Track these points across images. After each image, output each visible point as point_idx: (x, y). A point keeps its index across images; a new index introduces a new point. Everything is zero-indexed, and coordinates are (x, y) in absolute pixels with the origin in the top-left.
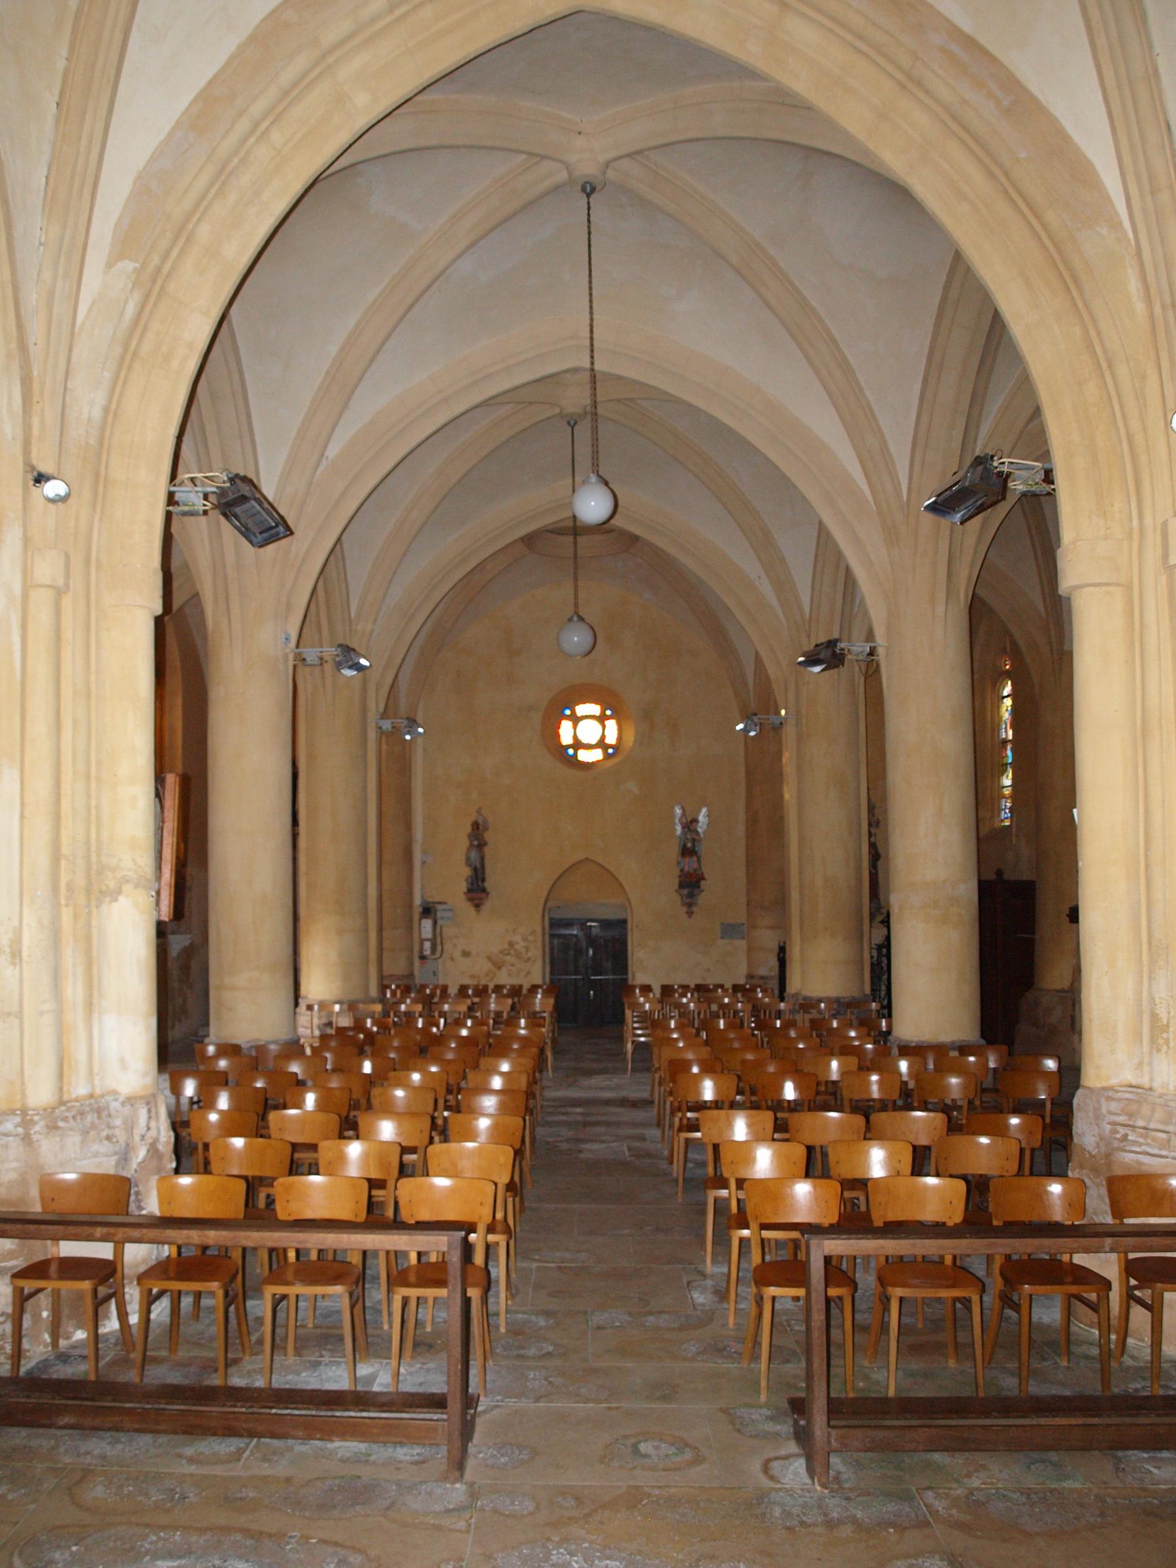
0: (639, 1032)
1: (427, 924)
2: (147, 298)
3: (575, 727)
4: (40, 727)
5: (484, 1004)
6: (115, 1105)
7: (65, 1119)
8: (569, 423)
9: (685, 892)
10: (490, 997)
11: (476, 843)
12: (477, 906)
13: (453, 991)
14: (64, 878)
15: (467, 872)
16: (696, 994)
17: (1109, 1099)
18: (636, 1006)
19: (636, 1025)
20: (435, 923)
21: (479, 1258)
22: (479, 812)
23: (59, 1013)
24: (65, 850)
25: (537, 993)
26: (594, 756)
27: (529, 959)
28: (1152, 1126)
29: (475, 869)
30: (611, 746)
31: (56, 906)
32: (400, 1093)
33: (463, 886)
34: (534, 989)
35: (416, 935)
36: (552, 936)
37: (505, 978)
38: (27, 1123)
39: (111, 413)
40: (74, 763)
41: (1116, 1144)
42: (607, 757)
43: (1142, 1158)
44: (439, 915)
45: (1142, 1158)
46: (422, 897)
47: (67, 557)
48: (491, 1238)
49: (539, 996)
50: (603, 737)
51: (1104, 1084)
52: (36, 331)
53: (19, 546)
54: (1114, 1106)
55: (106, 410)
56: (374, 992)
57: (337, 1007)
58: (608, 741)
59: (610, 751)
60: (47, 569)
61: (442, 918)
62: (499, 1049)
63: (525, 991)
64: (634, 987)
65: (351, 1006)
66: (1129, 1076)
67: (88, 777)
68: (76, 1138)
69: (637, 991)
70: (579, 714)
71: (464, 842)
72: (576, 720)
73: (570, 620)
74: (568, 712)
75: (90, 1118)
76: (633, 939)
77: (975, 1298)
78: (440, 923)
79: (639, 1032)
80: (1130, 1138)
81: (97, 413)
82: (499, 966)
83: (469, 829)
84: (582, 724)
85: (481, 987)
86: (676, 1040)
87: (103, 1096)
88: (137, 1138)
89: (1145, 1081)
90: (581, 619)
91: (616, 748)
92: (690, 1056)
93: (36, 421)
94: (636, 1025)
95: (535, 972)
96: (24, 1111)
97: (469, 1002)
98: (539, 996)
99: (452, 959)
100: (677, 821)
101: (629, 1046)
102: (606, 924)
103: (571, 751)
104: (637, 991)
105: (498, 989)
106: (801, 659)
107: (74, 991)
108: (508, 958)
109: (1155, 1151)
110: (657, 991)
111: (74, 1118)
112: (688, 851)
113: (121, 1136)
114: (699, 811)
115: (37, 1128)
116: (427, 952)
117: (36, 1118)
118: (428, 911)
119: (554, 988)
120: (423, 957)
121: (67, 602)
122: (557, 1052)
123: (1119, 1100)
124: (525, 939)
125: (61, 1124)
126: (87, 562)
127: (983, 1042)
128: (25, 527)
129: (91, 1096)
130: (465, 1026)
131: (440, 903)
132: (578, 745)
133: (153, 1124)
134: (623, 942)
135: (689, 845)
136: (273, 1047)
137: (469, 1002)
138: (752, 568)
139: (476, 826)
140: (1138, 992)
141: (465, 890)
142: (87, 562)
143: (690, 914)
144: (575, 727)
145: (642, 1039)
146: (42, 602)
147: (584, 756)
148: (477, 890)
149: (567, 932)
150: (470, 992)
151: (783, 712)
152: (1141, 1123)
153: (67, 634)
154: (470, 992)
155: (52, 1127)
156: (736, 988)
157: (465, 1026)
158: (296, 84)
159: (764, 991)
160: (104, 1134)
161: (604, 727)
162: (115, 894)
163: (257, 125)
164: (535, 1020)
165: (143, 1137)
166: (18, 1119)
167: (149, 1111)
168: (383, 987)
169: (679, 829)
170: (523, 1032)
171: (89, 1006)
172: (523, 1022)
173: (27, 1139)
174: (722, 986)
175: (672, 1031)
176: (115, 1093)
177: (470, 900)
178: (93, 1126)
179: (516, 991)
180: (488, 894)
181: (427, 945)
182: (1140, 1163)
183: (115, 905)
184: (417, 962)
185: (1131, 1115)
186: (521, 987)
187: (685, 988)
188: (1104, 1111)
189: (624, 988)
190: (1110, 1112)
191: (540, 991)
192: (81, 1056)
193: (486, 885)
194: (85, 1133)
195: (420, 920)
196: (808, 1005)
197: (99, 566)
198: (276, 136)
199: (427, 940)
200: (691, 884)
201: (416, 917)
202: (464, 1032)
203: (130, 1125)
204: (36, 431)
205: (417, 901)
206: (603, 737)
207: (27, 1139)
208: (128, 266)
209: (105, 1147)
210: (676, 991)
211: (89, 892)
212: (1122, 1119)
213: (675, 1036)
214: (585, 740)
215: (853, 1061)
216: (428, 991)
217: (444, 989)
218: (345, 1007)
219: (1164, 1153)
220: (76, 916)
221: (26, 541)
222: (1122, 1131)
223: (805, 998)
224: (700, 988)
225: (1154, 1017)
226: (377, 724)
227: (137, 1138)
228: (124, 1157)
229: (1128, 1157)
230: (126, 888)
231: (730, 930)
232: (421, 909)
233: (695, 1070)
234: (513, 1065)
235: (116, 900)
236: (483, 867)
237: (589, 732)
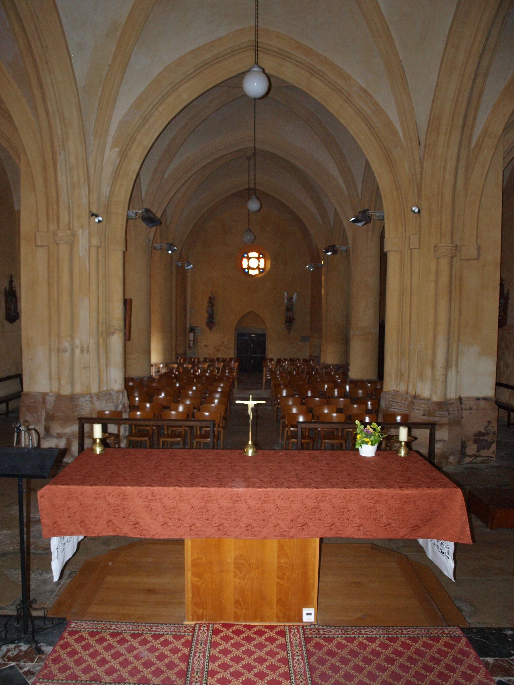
0: (268, 375)
1: (192, 335)
2: (122, 157)
3: (248, 261)
4: (93, 287)
5: (213, 365)
6: (113, 393)
7: (102, 396)
8: (248, 159)
9: (287, 324)
10: (215, 362)
11: (210, 305)
12: (210, 328)
13: (202, 360)
14: (100, 329)
15: (207, 315)
16: (289, 362)
17: (389, 394)
18: (267, 366)
19: (267, 373)
20: (194, 334)
21: (216, 433)
22: (212, 293)
23: (99, 367)
24: (100, 321)
25: (232, 361)
26: (256, 272)
27: (229, 348)
28: (398, 401)
29: (210, 315)
30: (262, 269)
31: (98, 338)
32: (190, 392)
33: (205, 321)
34: (231, 359)
35: (187, 339)
36: (238, 340)
37: (220, 355)
38: (91, 397)
39: (112, 193)
40: (103, 297)
41: (389, 406)
42: (260, 272)
43: (395, 410)
44: (196, 331)
45: (395, 410)
46: (190, 324)
47: (101, 238)
48: (219, 429)
49: (233, 362)
50: (259, 265)
51: (388, 390)
52: (92, 171)
53: (88, 235)
54: (390, 396)
55: (110, 192)
56: (174, 360)
57: (161, 366)
58: (260, 267)
59: (261, 270)
60: (95, 241)
61: (197, 333)
62: (220, 379)
63: (227, 360)
64: (267, 360)
65: (166, 365)
66: (394, 388)
67: (106, 300)
68: (105, 402)
69: (268, 361)
70: (250, 256)
71: (206, 304)
72: (249, 258)
73: (247, 231)
74: (246, 255)
75: (108, 396)
76: (268, 341)
77: (344, 443)
78: (196, 334)
79: (268, 375)
80: (393, 404)
81: (108, 194)
82: (218, 351)
83: (208, 300)
84: (251, 260)
85: (212, 358)
86: (278, 378)
87: (110, 390)
88: (119, 402)
89: (398, 389)
90: (250, 231)
91: (263, 269)
92: (281, 382)
93: (91, 197)
94: (267, 373)
95: (231, 353)
96: (90, 394)
97: (208, 364)
98: (233, 362)
99: (201, 348)
100: (285, 298)
101: (264, 380)
102: (258, 335)
103: (246, 270)
104: (268, 361)
105: (218, 359)
106: (324, 250)
107: (103, 361)
108: (222, 348)
109: (398, 408)
110: (275, 360)
111: (104, 396)
112: (289, 309)
113: (115, 401)
114: (294, 294)
115: (94, 399)
116: (192, 345)
117: (94, 396)
118: (192, 330)
119: (239, 359)
120: (190, 347)
121: (100, 250)
122: (239, 382)
123: (392, 394)
124: (228, 341)
125: (101, 398)
126: (105, 239)
127: (378, 380)
128: (89, 229)
129: (107, 390)
130: (207, 372)
131: (196, 327)
132: (249, 268)
133: (124, 398)
134: (264, 342)
135: (289, 307)
136: (145, 379)
137: (208, 364)
138: (313, 208)
139: (210, 298)
140: (398, 365)
141: (206, 322)
142: (105, 239)
143: (289, 332)
144: (248, 261)
145: (269, 378)
146: (93, 250)
147: (251, 272)
148: (211, 323)
149: (243, 338)
150: (208, 360)
151: (323, 262)
152: (396, 401)
153: (100, 259)
154: (208, 360)
155: (98, 399)
156: (304, 360)
157: (207, 372)
158: (166, 94)
159: (313, 361)
160: (111, 400)
161: (259, 261)
162: (114, 333)
163: (155, 106)
164: (231, 371)
165: (121, 402)
166: (89, 396)
167: (123, 395)
168: (177, 358)
169: (286, 300)
170: (227, 374)
171: (107, 365)
172: (227, 371)
173: (92, 402)
174: (299, 359)
175: (278, 375)
176: (113, 390)
177: (208, 326)
178: (109, 399)
179: (224, 360)
180: (214, 324)
181: (192, 343)
182: (394, 411)
183: (113, 337)
184: (188, 349)
185: (394, 398)
186: (226, 358)
187: (286, 360)
188: (387, 397)
189: (264, 359)
190: (389, 398)
191: (233, 360)
192: (105, 379)
193: (214, 320)
194: (106, 400)
195: (189, 333)
196: (327, 367)
197: (108, 238)
198: (160, 109)
199: (192, 341)
200: (290, 321)
201: (187, 331)
202: (207, 374)
203: (118, 398)
204: (91, 200)
205: (188, 326)
206: (259, 265)
207: (92, 402)
208: (117, 149)
209: (112, 405)
210: (282, 361)
211: (106, 333)
212: (392, 399)
213: (278, 376)
214: (252, 266)
215: (332, 385)
216: (192, 360)
217: (198, 359)
218: (164, 365)
219: (400, 408)
220: (103, 340)
221: (89, 233)
222: (391, 403)
223: (327, 364)
224: (291, 360)
225: (401, 372)
226: (176, 264)
227: (119, 402)
228: (117, 406)
229: (392, 410)
230: (117, 332)
231: (304, 339)
232: (189, 329)
233: (282, 387)
234: (224, 384)
235: (113, 335)
236: (213, 314)
237: (253, 263)
